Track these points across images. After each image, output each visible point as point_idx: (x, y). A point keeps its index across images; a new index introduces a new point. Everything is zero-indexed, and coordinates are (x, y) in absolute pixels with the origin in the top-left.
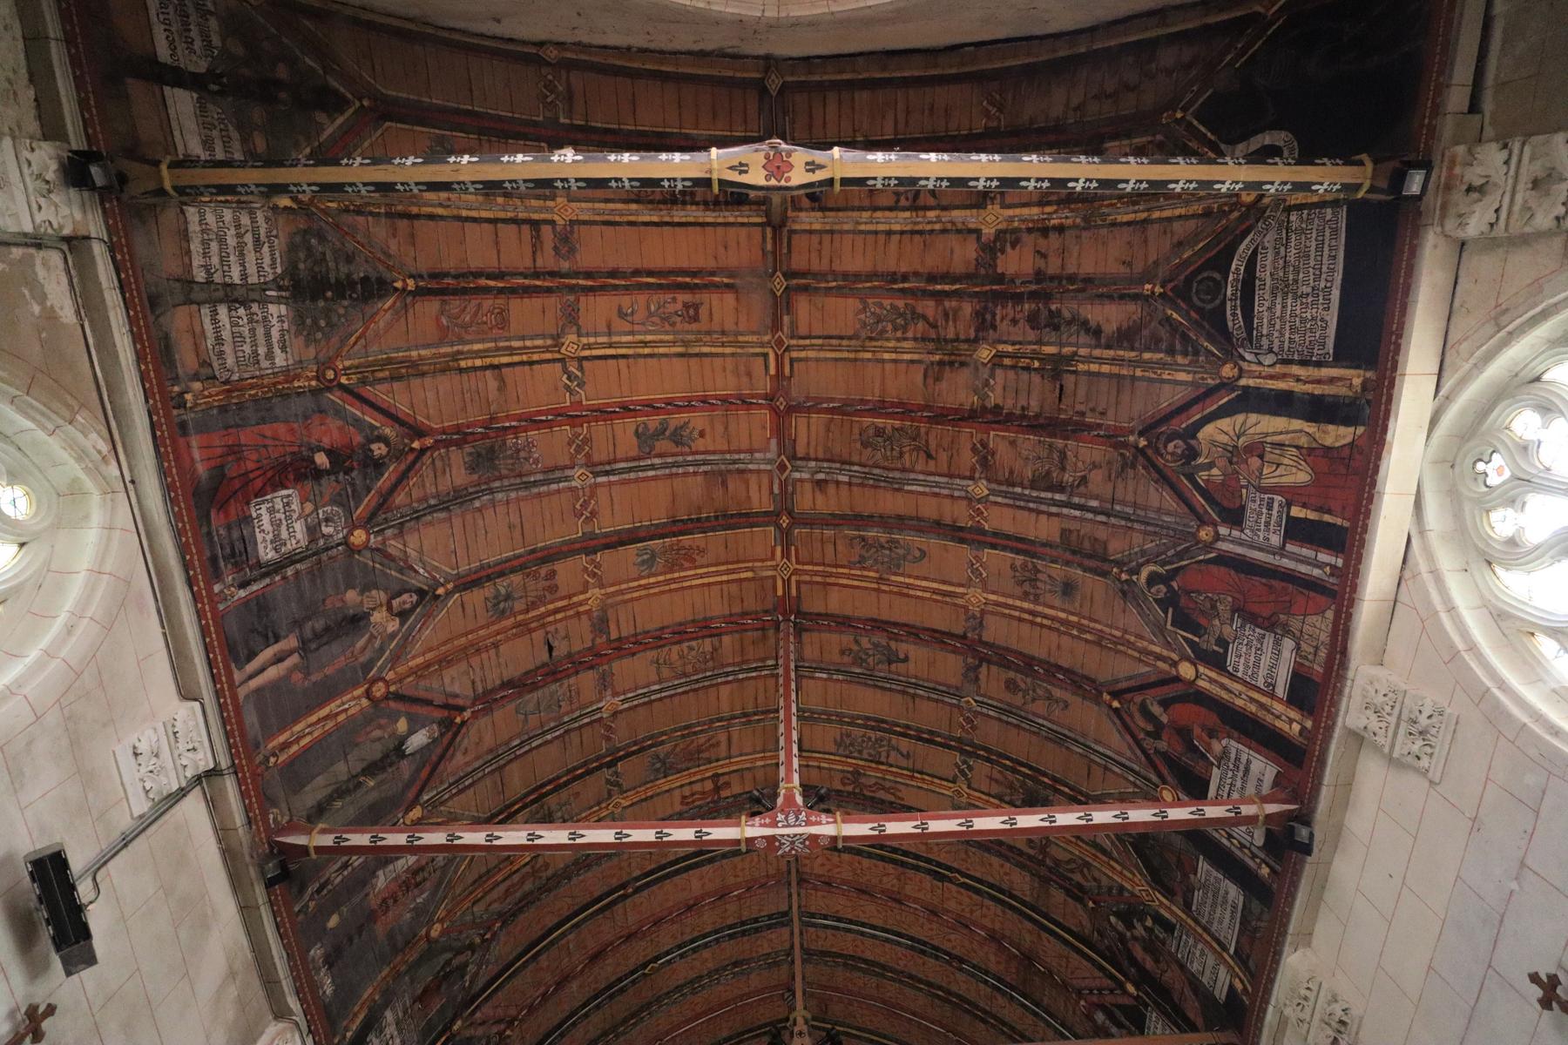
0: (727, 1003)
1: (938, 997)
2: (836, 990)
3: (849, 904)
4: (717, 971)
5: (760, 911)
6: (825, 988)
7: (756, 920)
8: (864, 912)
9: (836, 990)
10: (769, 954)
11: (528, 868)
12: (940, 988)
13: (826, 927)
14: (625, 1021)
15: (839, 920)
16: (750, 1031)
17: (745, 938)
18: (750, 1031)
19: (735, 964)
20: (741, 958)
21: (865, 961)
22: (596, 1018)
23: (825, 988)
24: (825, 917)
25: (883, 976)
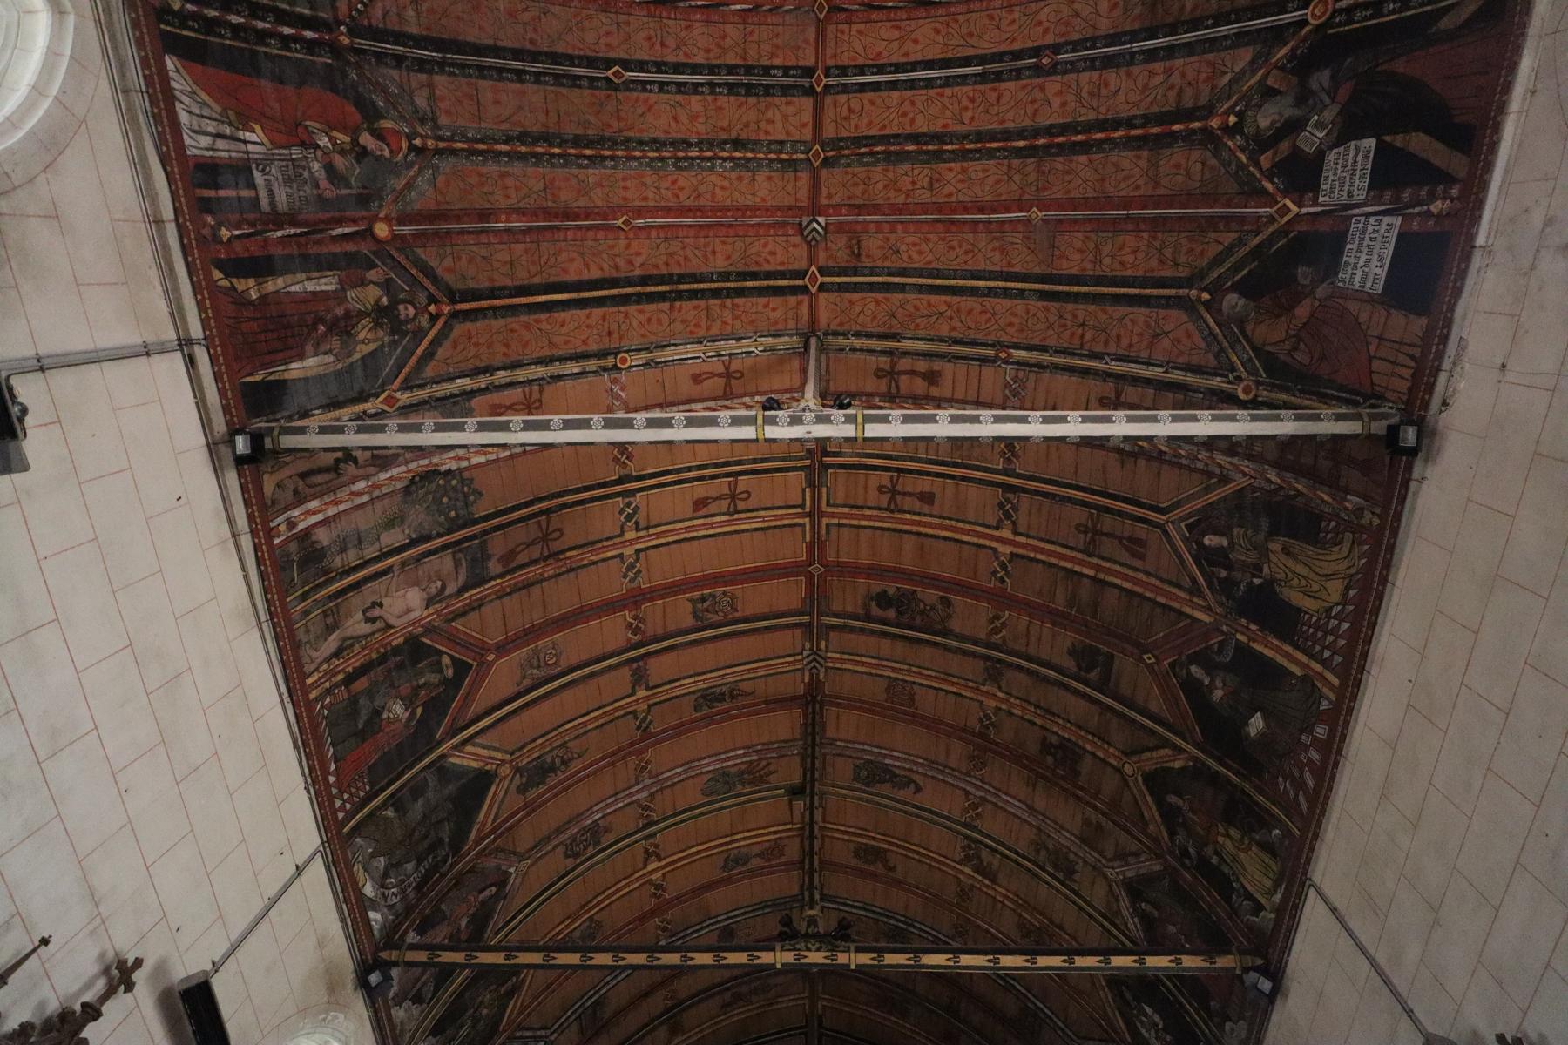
0: (724, 210)
1: (1019, 153)
2: (876, 209)
3: (897, 34)
4: (710, 144)
5: (773, 55)
6: (858, 209)
7: (766, 71)
8: (916, 41)
9: (876, 209)
10: (782, 143)
11: (612, 631)
12: (1020, 134)
13: (862, 87)
14: (577, 141)
15: (881, 69)
16: (754, 276)
17: (752, 100)
18: (754, 276)
19: (738, 144)
20: (744, 136)
21: (915, 138)
22: (534, 95)
23: (858, 209)
24: (861, 70)
25: (938, 156)
